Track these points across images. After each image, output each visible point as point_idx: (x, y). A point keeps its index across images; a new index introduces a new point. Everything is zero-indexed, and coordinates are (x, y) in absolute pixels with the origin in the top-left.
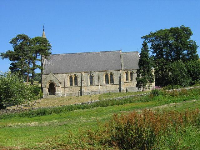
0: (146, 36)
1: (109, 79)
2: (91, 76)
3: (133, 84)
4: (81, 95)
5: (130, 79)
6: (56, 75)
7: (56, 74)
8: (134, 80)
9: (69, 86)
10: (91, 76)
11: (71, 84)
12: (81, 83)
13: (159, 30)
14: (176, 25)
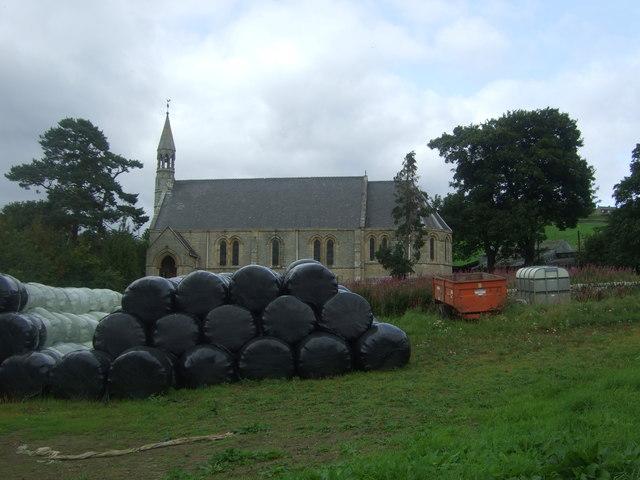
0: (445, 137)
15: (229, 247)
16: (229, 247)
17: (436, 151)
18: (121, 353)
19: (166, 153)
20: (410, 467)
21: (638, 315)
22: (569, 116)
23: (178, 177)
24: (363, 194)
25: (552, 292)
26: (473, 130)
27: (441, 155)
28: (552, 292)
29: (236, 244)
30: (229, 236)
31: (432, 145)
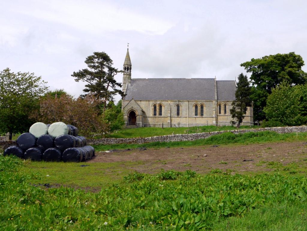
0: (247, 63)
1: (199, 111)
2: (178, 106)
3: (227, 119)
4: (304, 160)
5: (222, 111)
6: (139, 102)
7: (139, 101)
8: (247, 114)
9: (176, 116)
10: (178, 106)
11: (155, 114)
12: (220, 109)
13: (264, 56)
14: (284, 51)
15: (158, 108)
16: (158, 108)
17: (243, 68)
18: (46, 150)
19: (128, 68)
20: (14, 182)
21: (1, 134)
22: (295, 53)
23: (133, 77)
24: (215, 86)
25: (171, 121)
26: (258, 60)
27: (245, 69)
28: (171, 121)
29: (161, 106)
30: (158, 102)
31: (242, 65)
